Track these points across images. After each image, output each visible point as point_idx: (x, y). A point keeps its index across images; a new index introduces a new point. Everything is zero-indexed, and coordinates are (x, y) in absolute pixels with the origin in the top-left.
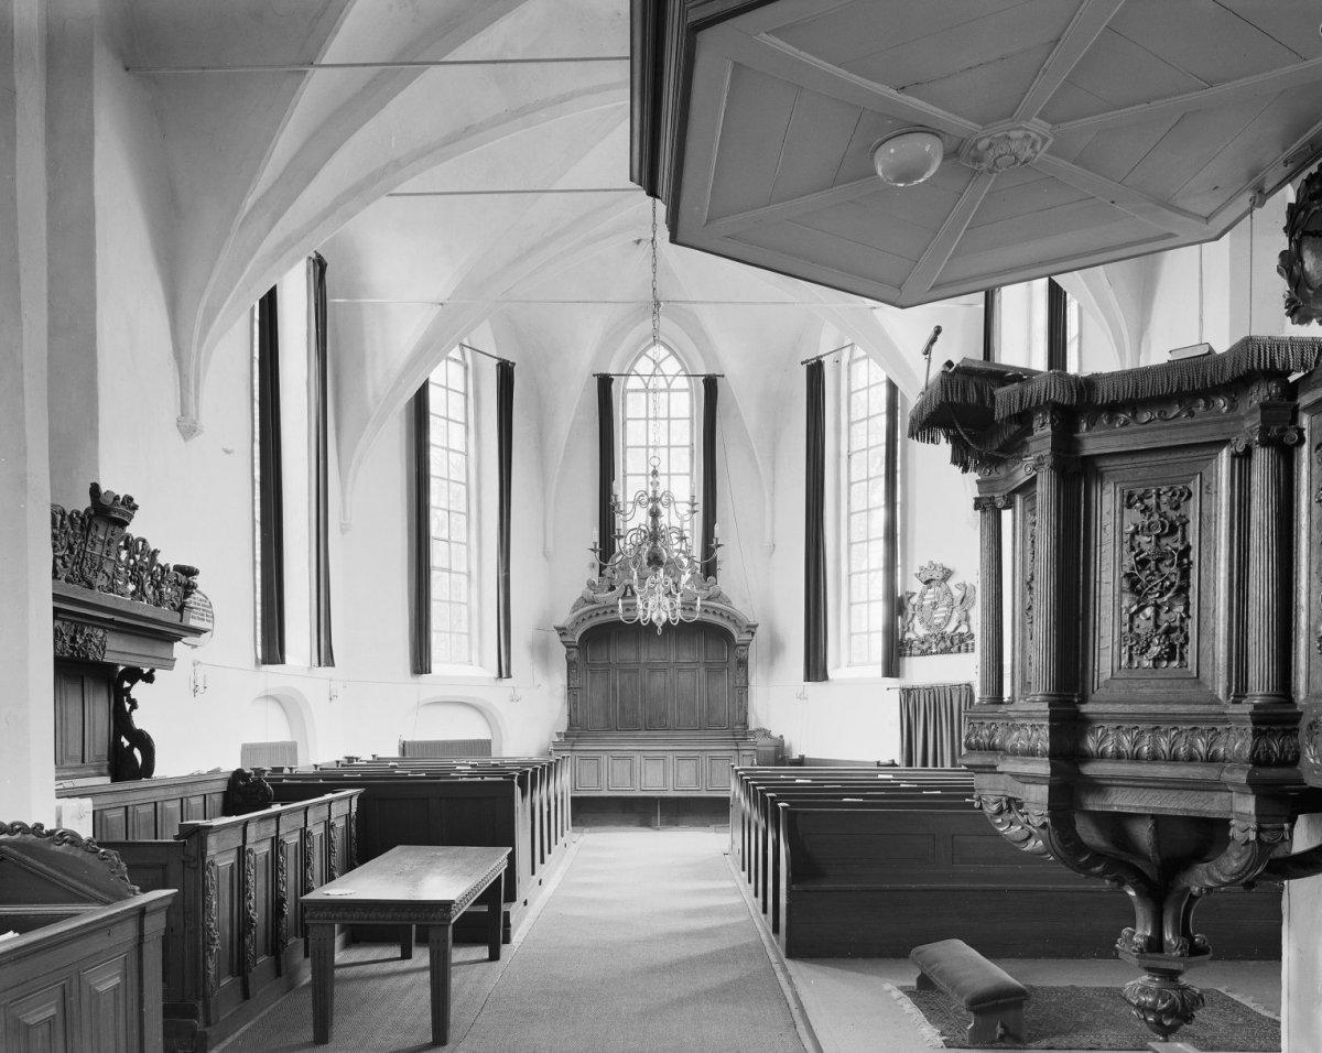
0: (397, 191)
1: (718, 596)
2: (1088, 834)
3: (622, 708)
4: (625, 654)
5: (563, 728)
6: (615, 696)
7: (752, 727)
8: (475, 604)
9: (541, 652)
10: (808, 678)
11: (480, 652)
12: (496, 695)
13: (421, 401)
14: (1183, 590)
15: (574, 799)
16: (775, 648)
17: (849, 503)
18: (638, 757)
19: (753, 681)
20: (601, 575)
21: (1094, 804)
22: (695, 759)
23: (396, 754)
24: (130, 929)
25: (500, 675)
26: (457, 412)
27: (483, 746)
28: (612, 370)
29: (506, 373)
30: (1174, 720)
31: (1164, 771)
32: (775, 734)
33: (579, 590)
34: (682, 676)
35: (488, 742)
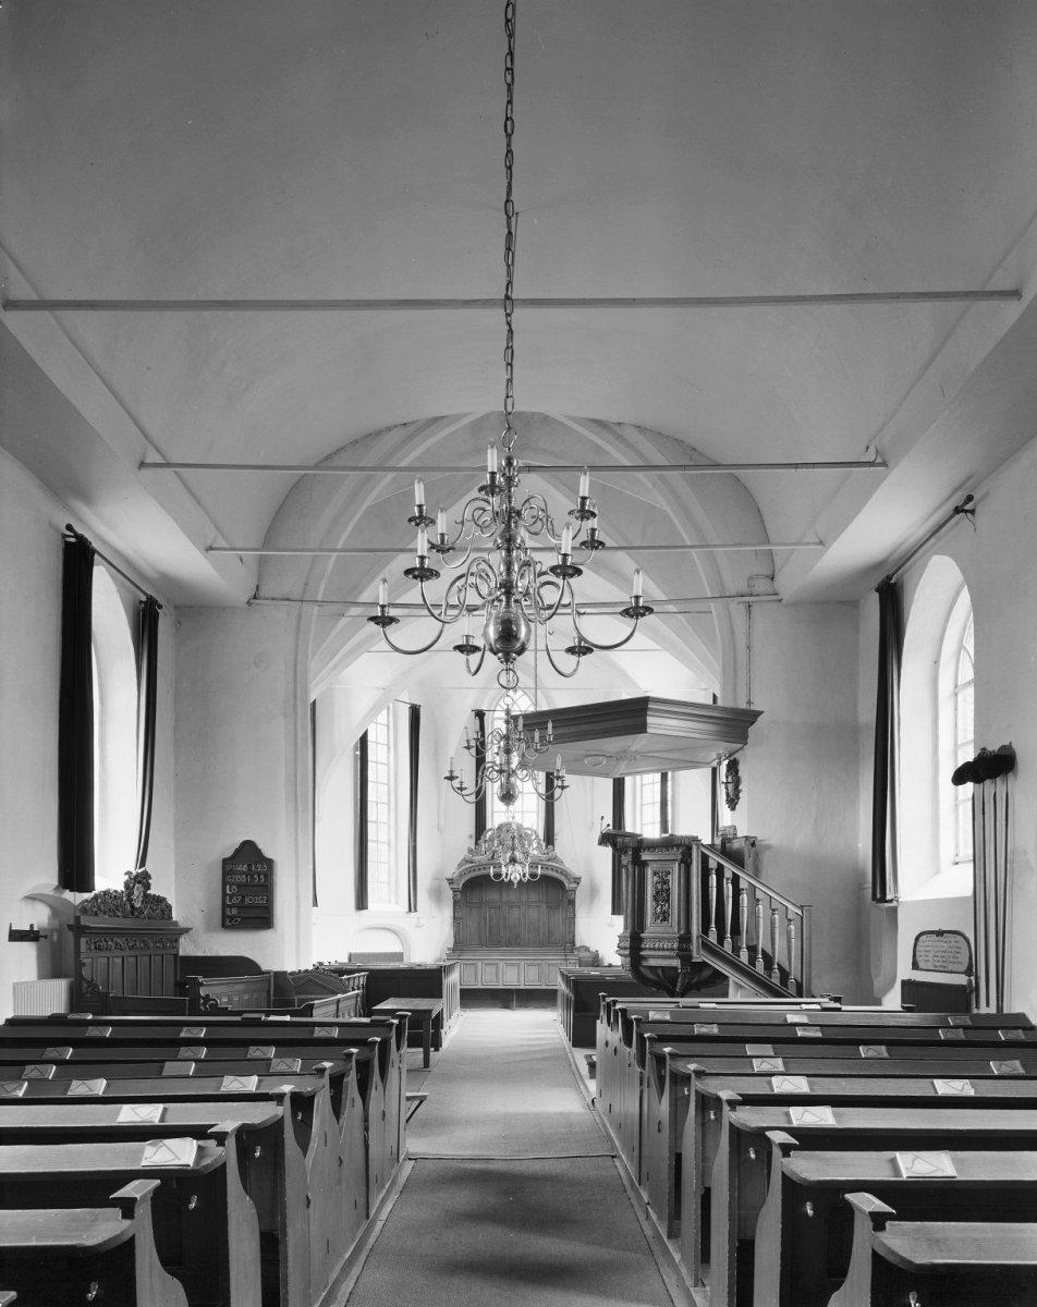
0: (373, 649)
1: (555, 859)
2: (648, 974)
3: (490, 932)
4: (493, 896)
5: (451, 945)
6: (485, 924)
7: (578, 944)
8: (393, 863)
9: (436, 894)
10: (613, 913)
11: (396, 894)
12: (407, 922)
13: (364, 740)
14: (668, 901)
15: (461, 990)
16: (594, 892)
17: (642, 797)
18: (501, 964)
19: (578, 914)
20: (476, 844)
21: (645, 964)
22: (538, 965)
23: (346, 961)
24: (334, 1007)
25: (410, 910)
26: (383, 739)
27: (399, 956)
28: (484, 708)
29: (415, 713)
30: (664, 939)
31: (661, 953)
32: (593, 949)
33: (462, 854)
34: (531, 910)
35: (402, 954)
